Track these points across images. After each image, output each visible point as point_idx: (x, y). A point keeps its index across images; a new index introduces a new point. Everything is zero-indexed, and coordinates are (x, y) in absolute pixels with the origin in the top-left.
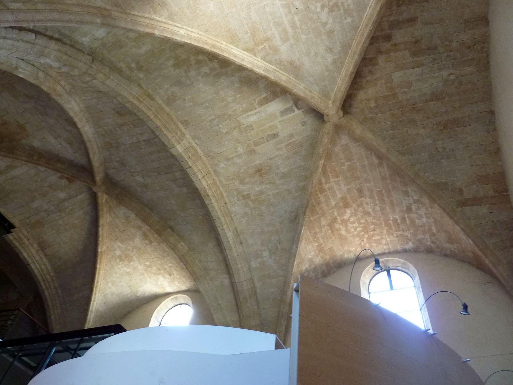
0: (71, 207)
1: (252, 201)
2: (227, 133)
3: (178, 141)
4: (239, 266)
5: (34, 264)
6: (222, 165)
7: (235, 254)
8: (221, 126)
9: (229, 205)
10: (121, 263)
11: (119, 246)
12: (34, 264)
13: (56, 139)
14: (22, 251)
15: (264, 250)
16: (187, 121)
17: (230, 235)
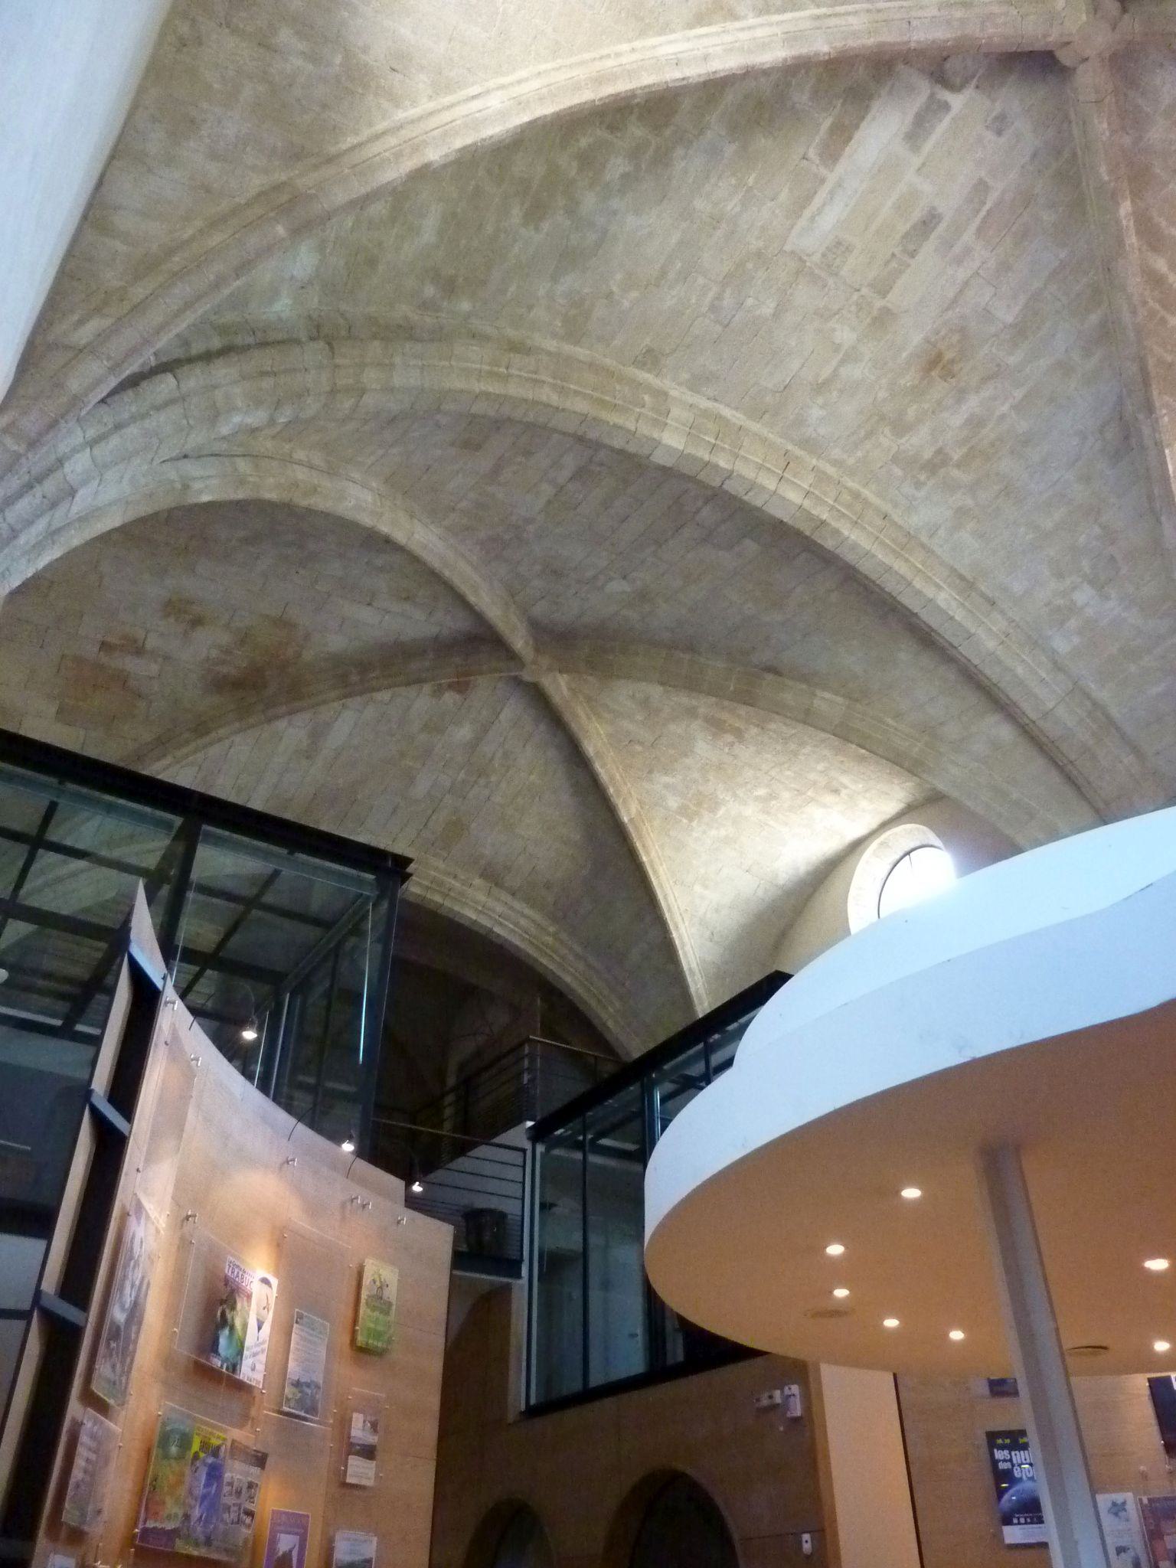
1: (958, 466)
2: (777, 315)
5: (501, 924)
7: (991, 644)
8: (750, 302)
10: (694, 823)
11: (667, 786)
14: (457, 908)
16: (650, 351)
17: (945, 598)
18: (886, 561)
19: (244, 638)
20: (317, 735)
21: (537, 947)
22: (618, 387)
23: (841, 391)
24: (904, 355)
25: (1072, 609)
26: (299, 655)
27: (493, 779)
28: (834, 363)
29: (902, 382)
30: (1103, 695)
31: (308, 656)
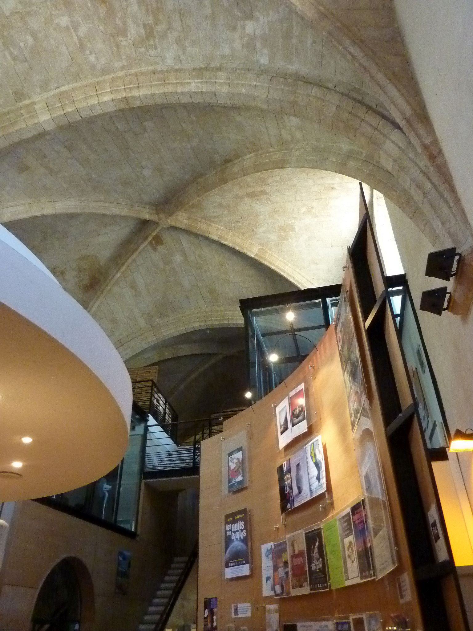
1: (157, 24)
2: (35, 38)
3: (32, 117)
4: (244, 91)
6: (92, 58)
7: (225, 89)
8: (22, 44)
9: (159, 68)
10: (290, 240)
11: (265, 232)
15: (244, 28)
16: (16, 93)
17: (194, 86)
18: (161, 91)
19: (80, 270)
20: (133, 286)
22: (8, 117)
23: (89, 41)
24: (89, 5)
25: (253, 38)
26: (99, 265)
28: (74, 35)
29: (102, 15)
30: (291, 68)
31: (102, 262)
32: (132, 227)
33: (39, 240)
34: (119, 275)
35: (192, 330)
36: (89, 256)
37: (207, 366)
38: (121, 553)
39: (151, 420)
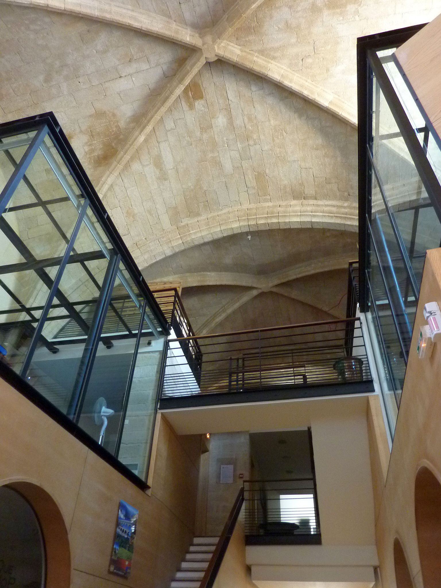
0: (246, 118)
5: (314, 216)
12: (314, 216)
13: (121, 77)
14: (287, 220)
20: (158, 163)
21: (341, 217)
26: (117, 126)
27: (255, 136)
31: (122, 124)
32: (165, 67)
33: (41, 78)
34: (142, 138)
35: (230, 233)
36: (105, 113)
37: (237, 305)
38: (122, 506)
39: (173, 335)
